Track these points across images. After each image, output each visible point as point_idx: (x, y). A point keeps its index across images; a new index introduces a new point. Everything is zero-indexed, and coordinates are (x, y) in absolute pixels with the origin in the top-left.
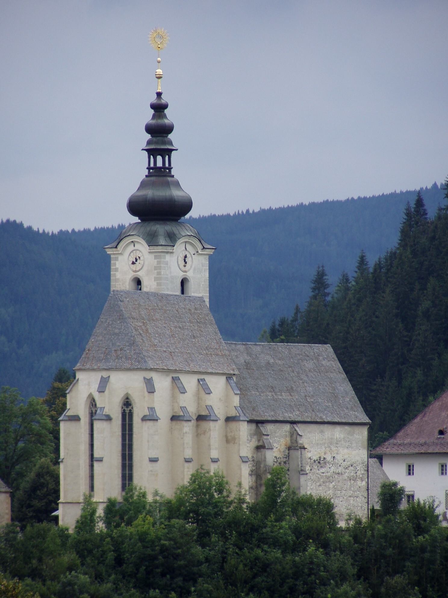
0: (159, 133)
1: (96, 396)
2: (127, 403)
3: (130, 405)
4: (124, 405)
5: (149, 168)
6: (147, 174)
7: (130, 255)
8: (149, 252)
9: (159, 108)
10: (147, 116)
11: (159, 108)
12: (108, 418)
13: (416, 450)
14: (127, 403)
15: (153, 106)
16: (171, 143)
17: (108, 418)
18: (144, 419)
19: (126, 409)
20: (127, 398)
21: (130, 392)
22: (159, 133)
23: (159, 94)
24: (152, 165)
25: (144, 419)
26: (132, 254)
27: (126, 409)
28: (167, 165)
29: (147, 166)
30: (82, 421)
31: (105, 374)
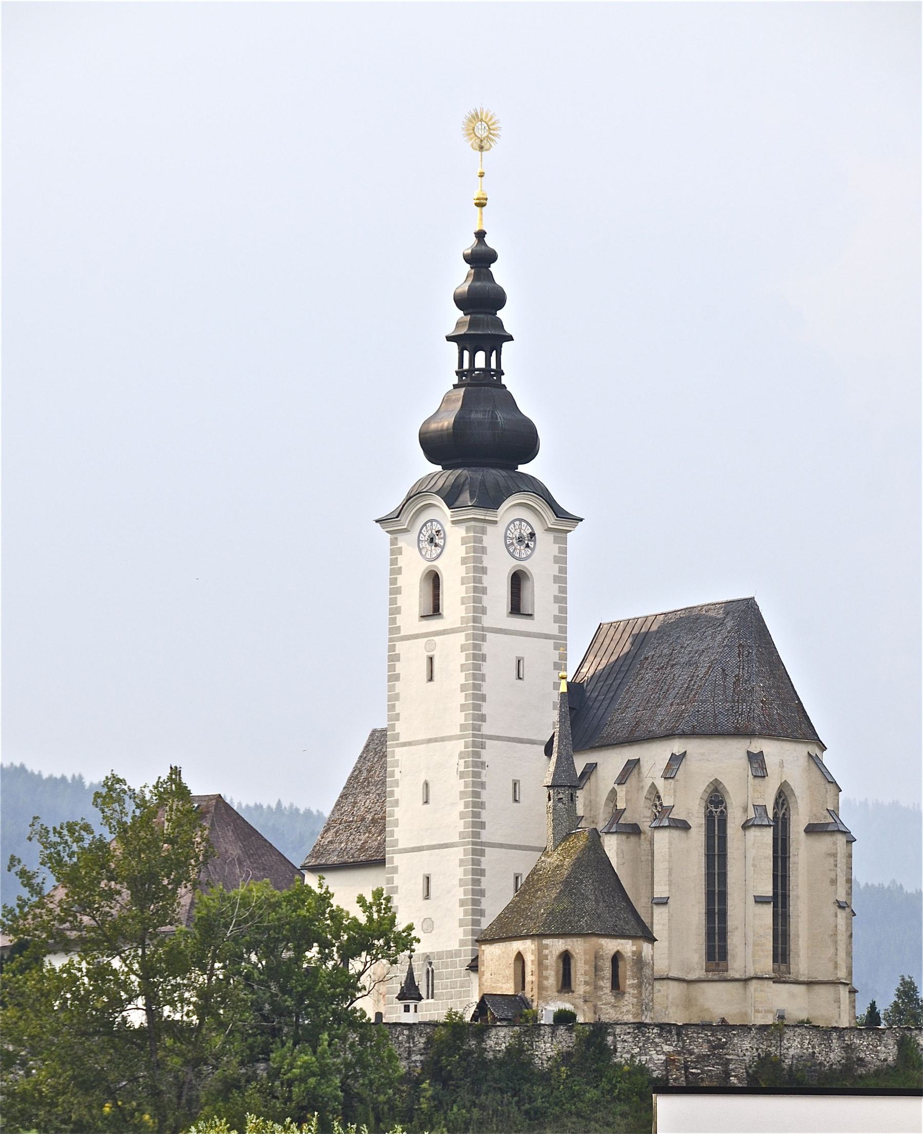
0: (482, 305)
1: (660, 784)
2: (716, 799)
3: (722, 802)
4: (711, 802)
5: (460, 373)
6: (456, 382)
7: (420, 532)
8: (454, 522)
9: (481, 259)
10: (460, 276)
11: (481, 259)
12: (683, 826)
13: (780, 892)
14: (716, 799)
15: (468, 259)
16: (499, 324)
17: (683, 826)
18: (812, 830)
19: (714, 810)
20: (716, 790)
21: (24, 762)
22: (482, 305)
23: (481, 235)
24: (466, 366)
25: (812, 830)
26: (512, 526)
27: (714, 810)
28: (493, 366)
29: (456, 367)
30: (693, 830)
31: (676, 746)
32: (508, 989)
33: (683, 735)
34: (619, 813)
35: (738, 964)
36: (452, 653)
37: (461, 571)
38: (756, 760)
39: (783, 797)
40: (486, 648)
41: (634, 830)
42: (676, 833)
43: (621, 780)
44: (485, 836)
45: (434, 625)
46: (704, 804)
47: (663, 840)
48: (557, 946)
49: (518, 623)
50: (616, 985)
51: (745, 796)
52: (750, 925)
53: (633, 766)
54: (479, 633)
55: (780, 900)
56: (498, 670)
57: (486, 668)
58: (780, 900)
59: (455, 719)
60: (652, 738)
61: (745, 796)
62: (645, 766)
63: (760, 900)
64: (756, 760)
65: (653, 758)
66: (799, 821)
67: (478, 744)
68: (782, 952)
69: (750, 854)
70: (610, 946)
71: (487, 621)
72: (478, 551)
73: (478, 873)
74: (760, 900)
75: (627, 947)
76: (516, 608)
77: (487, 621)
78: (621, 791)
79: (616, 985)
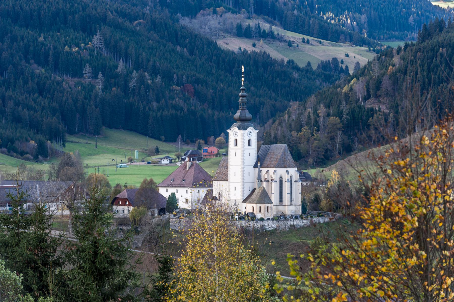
1: (273, 175)
12: (276, 181)
17: (276, 181)
31: (275, 169)
32: (251, 211)
33: (276, 167)
34: (266, 179)
35: (284, 203)
36: (239, 153)
37: (241, 140)
38: (287, 171)
39: (291, 177)
40: (245, 152)
41: (268, 181)
42: (275, 183)
43: (266, 173)
44: (245, 181)
45: (236, 147)
46: (293, 214)
47: (273, 184)
48: (259, 205)
49: (250, 147)
50: (268, 211)
51: (286, 177)
52: (286, 198)
53: (268, 171)
54: (244, 150)
55: (291, 193)
56: (246, 155)
57: (245, 155)
58: (291, 193)
59: (240, 163)
60: (271, 167)
61: (286, 177)
62: (270, 171)
63: (288, 194)
64: (287, 171)
65: (271, 170)
66: (294, 180)
67: (244, 167)
68: (291, 201)
69: (286, 186)
70: (267, 205)
71: (245, 148)
72: (243, 136)
73: (244, 187)
74: (288, 194)
75: (269, 205)
76: (249, 145)
77: (245, 148)
78: (266, 175)
79: (268, 211)
